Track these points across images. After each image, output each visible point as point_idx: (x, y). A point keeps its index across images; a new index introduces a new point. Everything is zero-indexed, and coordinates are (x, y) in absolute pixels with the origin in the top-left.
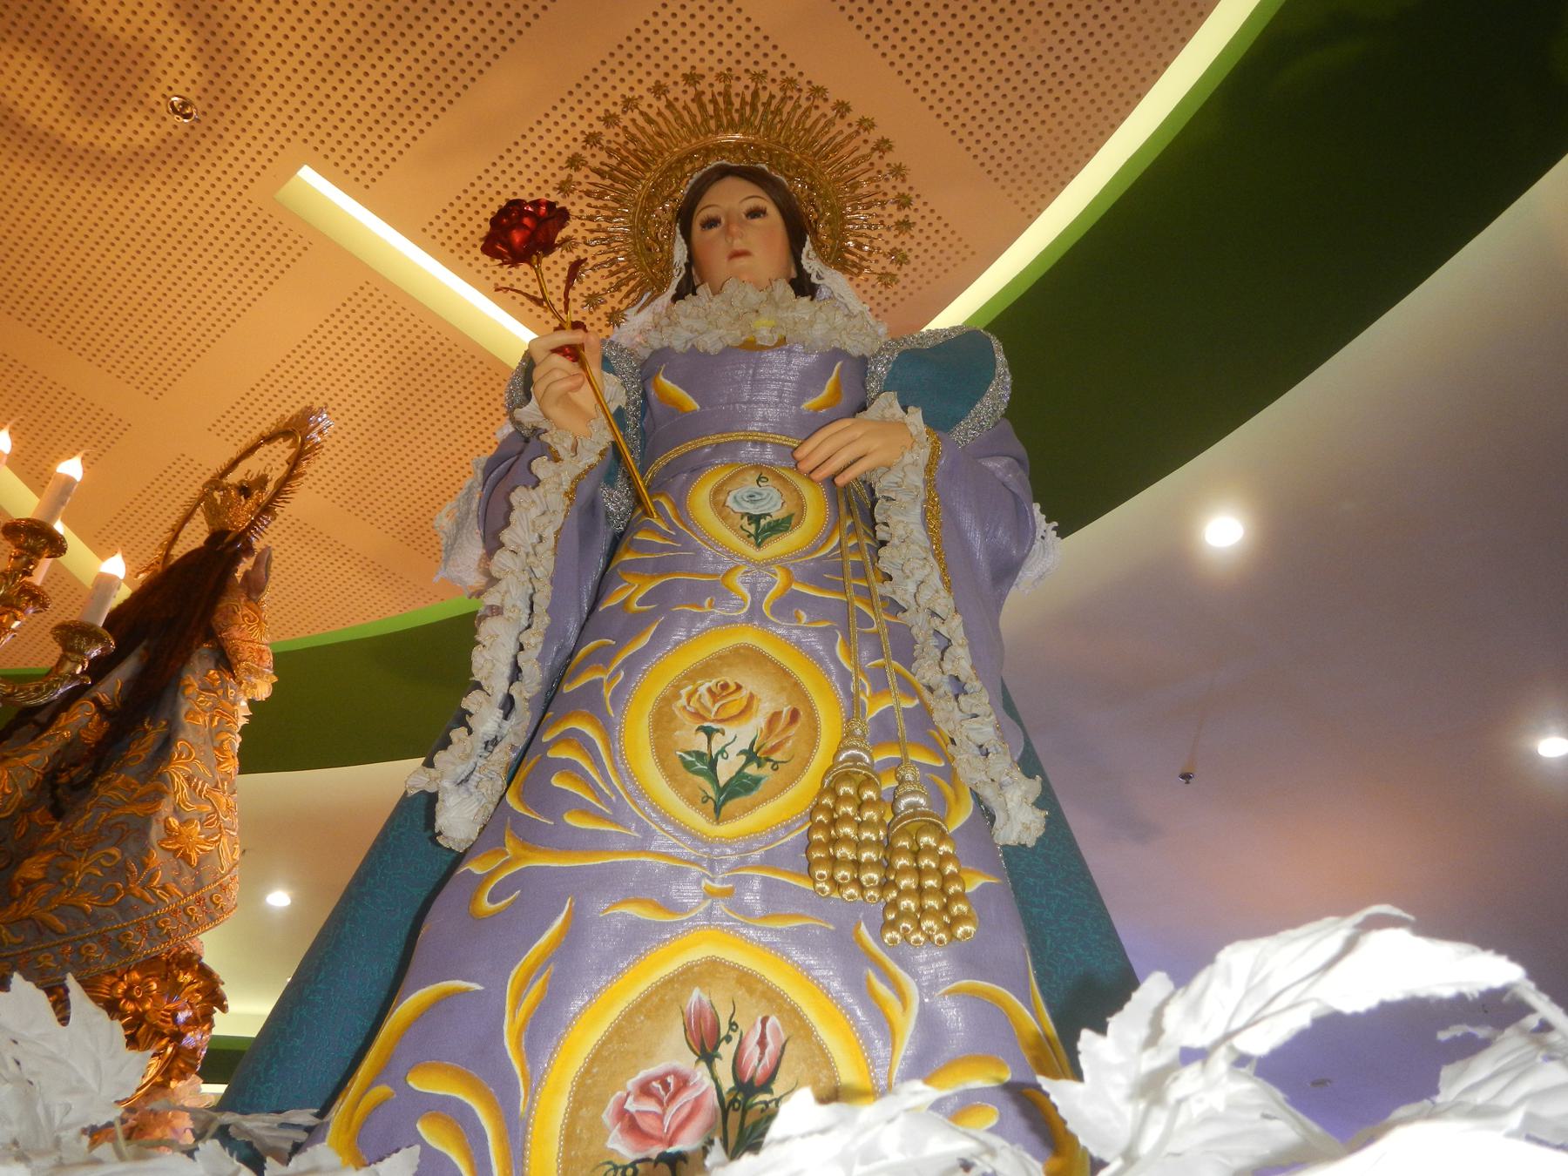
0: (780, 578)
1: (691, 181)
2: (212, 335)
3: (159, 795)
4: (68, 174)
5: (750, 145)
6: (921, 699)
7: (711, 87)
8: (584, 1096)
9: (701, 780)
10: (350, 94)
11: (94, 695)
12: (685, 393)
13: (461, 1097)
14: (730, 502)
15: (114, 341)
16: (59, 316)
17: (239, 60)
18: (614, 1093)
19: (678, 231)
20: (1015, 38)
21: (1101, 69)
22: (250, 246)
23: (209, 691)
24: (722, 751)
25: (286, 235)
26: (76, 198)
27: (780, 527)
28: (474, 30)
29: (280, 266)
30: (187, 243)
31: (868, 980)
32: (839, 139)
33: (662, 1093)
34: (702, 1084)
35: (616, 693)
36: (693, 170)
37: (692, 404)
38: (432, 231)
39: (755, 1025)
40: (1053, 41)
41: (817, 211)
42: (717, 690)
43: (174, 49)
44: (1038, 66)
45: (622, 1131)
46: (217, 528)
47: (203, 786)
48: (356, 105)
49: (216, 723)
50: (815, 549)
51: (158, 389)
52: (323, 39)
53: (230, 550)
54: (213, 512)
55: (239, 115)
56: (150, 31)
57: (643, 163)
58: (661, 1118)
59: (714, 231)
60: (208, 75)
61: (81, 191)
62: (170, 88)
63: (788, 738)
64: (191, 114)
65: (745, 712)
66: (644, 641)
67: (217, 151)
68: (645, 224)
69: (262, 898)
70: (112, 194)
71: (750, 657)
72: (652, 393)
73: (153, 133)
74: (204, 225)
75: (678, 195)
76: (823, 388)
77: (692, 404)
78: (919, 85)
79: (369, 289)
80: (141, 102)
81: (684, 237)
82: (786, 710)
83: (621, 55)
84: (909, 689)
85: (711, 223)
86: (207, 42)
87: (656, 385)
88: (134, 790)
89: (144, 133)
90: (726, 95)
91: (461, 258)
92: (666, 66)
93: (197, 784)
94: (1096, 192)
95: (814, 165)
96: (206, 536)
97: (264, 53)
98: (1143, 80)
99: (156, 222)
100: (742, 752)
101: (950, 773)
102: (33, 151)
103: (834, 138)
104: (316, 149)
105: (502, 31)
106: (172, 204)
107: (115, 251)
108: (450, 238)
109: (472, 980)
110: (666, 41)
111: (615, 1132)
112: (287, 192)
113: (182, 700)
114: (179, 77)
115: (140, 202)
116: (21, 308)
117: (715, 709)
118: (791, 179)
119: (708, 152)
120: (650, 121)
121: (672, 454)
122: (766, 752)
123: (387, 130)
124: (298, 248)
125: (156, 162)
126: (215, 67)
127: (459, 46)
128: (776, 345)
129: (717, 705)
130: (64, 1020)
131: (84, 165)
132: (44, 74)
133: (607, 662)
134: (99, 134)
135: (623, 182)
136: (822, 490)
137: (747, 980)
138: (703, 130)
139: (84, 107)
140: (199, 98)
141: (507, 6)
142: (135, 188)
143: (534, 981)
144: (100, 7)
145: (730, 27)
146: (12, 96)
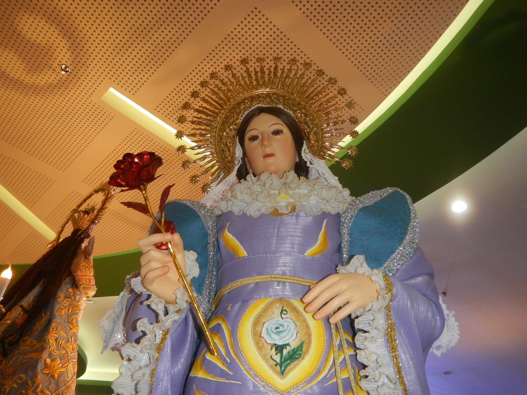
1: (244, 116)
2: (81, 149)
3: (42, 349)
4: (26, 94)
5: (274, 94)
7: (253, 65)
10: (143, 55)
11: (21, 304)
12: (239, 244)
14: (264, 334)
15: (46, 154)
17: (84, 50)
19: (238, 141)
20: (380, 28)
21: (421, 38)
22: (93, 117)
23: (68, 298)
25: (105, 113)
26: (30, 102)
29: (104, 124)
30: (70, 117)
32: (319, 89)
36: (245, 109)
37: (243, 252)
38: (158, 109)
40: (395, 28)
41: (309, 128)
43: (60, 47)
44: (389, 38)
46: (76, 228)
47: (62, 342)
48: (128, 65)
49: (70, 311)
50: (319, 372)
51: (63, 168)
53: (79, 238)
54: (75, 222)
55: (86, 70)
56: (51, 41)
59: (256, 142)
60: (74, 56)
61: (31, 100)
64: (68, 71)
67: (79, 83)
68: (221, 138)
70: (42, 100)
72: (221, 241)
74: (76, 110)
76: (317, 240)
77: (243, 252)
78: (322, 28)
79: (136, 131)
80: (50, 67)
83: (226, 42)
85: (254, 138)
86: (72, 44)
88: (34, 345)
89: (52, 78)
91: (169, 119)
92: (231, 57)
93: (59, 342)
95: (307, 103)
97: (93, 47)
99: (59, 110)
102: (13, 86)
104: (114, 81)
106: (64, 103)
107: (45, 120)
112: (107, 94)
113: (56, 304)
114: (63, 57)
115: (52, 103)
116: (14, 142)
118: (295, 111)
119: (252, 99)
120: (224, 84)
124: (110, 117)
125: (57, 89)
126: (76, 53)
127: (165, 41)
128: (290, 213)
131: (32, 91)
132: (15, 59)
134: (36, 79)
138: (250, 87)
139: (30, 70)
140: (71, 65)
142: (50, 98)
145: (267, 29)
146: (4, 67)
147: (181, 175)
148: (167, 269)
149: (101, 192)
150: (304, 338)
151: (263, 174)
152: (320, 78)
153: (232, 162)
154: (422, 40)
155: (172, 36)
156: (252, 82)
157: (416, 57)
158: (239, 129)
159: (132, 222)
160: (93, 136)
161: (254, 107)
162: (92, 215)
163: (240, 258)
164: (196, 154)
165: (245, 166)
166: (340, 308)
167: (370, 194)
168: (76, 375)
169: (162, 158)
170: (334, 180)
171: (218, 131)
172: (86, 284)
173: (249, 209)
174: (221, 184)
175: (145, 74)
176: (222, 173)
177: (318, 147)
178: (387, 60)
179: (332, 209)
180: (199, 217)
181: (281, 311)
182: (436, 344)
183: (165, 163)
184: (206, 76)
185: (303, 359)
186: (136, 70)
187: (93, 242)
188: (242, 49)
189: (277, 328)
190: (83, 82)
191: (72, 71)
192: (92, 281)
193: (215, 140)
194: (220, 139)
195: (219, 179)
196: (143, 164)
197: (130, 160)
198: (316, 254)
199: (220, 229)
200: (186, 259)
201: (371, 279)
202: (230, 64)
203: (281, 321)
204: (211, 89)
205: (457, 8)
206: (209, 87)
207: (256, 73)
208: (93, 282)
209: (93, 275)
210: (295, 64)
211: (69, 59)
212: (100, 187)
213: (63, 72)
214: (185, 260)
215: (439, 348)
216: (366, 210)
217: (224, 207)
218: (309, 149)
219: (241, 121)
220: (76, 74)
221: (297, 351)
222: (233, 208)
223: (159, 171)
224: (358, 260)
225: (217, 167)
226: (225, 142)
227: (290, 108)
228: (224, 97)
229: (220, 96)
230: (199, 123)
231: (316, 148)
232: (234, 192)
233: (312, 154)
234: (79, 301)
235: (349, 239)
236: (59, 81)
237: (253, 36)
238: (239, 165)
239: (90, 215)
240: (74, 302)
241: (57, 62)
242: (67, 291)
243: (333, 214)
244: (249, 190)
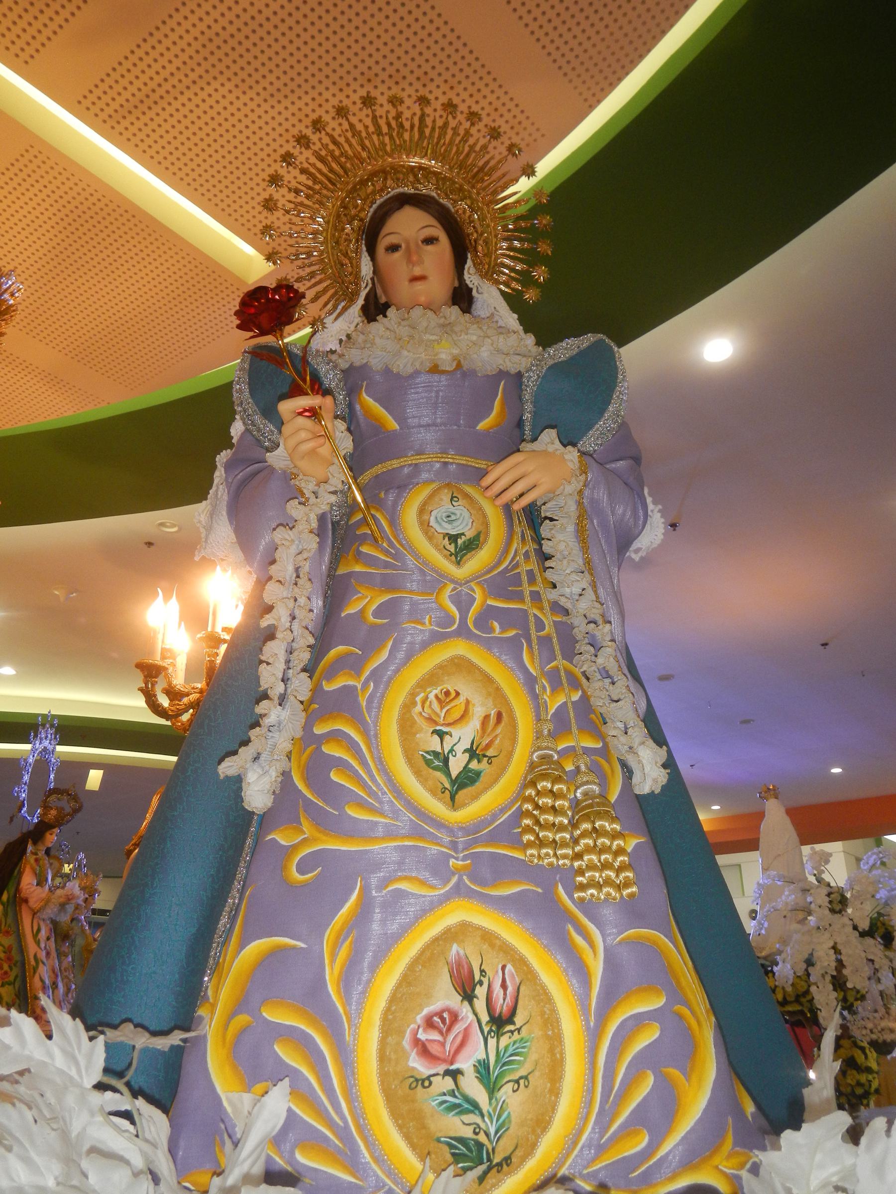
0: (478, 595)
1: (375, 206)
6: (584, 691)
8: (389, 1027)
9: (438, 774)
13: (303, 1027)
14: (433, 523)
18: (408, 1026)
19: (364, 248)
24: (452, 750)
27: (473, 545)
31: (568, 932)
32: (492, 163)
33: (442, 1026)
34: (468, 1017)
35: (370, 701)
39: (497, 972)
41: (477, 232)
42: (441, 696)
45: (417, 1053)
50: (499, 563)
58: (443, 1044)
59: (397, 255)
63: (496, 736)
65: (464, 716)
66: (384, 655)
68: (337, 243)
71: (460, 665)
72: (358, 407)
76: (492, 409)
77: (392, 424)
82: (493, 713)
84: (575, 684)
85: (393, 248)
91: (129, 140)
100: (465, 751)
101: (604, 751)
109: (298, 940)
111: (413, 1054)
117: (443, 715)
119: (384, 172)
120: (335, 142)
121: (378, 469)
122: (482, 750)
129: (444, 710)
130: (50, 1037)
133: (357, 670)
136: (500, 511)
137: (488, 936)
138: (381, 153)
143: (342, 943)
150: (481, 528)
152: (494, 143)
159: (25, 364)
166: (521, 495)
167: (564, 344)
170: (511, 320)
174: (340, 319)
175: (180, 107)
177: (489, 265)
182: (636, 545)
185: (481, 548)
189: (449, 516)
195: (338, 311)
198: (491, 428)
202: (344, 104)
203: (452, 509)
215: (637, 551)
216: (558, 369)
217: (355, 356)
221: (474, 540)
224: (549, 437)
231: (486, 266)
235: (533, 409)
238: (368, 289)
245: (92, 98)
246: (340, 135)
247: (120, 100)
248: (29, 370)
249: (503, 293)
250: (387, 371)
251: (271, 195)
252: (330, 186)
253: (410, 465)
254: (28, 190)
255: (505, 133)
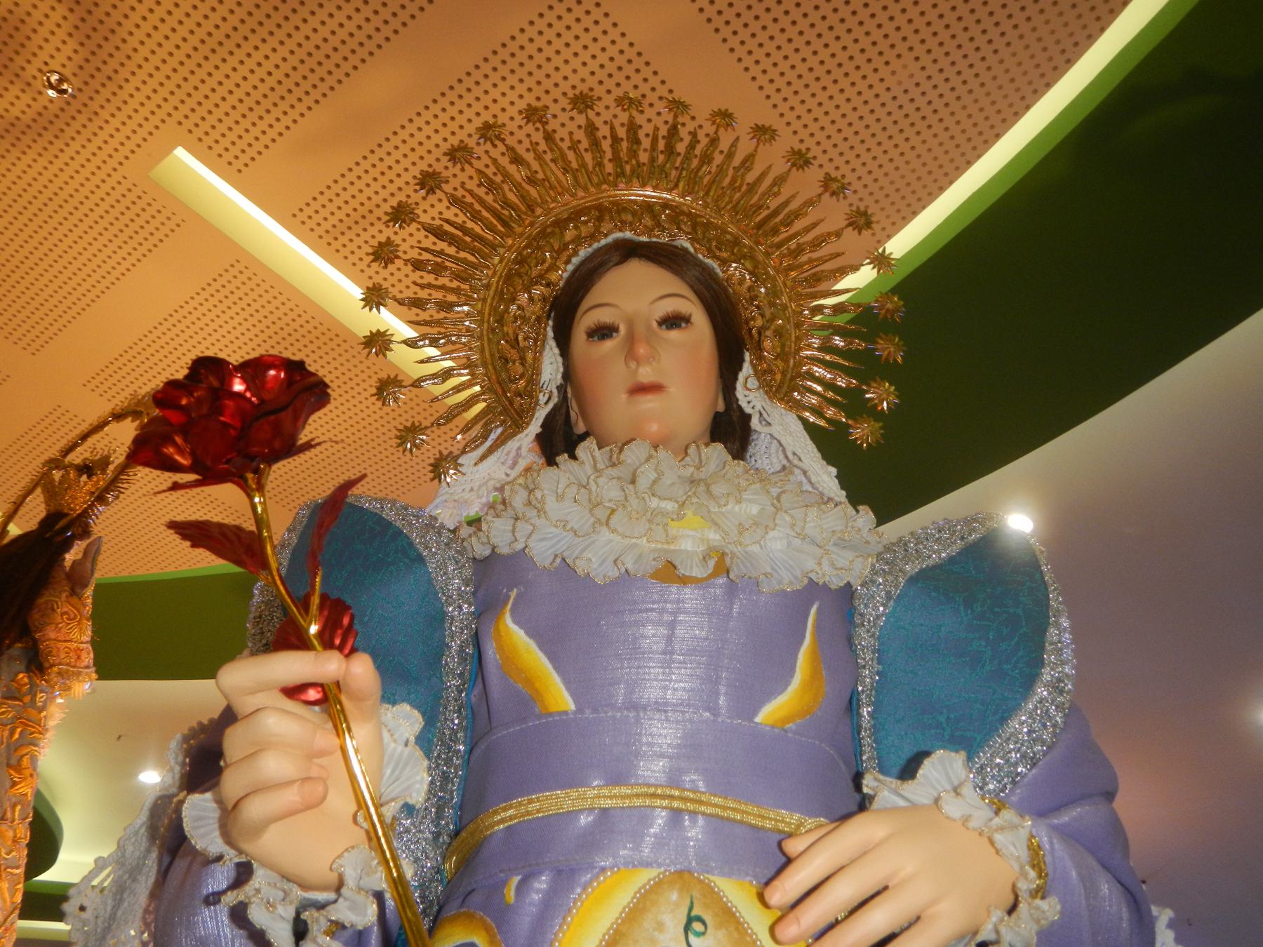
1: (575, 260)
7: (608, 115)
16: (43, 233)
17: (115, 40)
19: (550, 334)
28: (350, 26)
32: (793, 206)
36: (578, 241)
41: (763, 316)
43: (49, 25)
46: (52, 509)
49: (16, 736)
51: (35, 346)
52: (199, 25)
53: (59, 539)
54: (52, 493)
57: (504, 223)
59: (609, 345)
60: (84, 53)
62: (46, 64)
64: (65, 91)
67: (92, 127)
68: (500, 321)
69: (136, 775)
73: (29, 106)
75: (553, 277)
77: (560, 698)
79: (239, 267)
80: (17, 75)
81: (559, 345)
83: (495, 61)
85: (603, 332)
87: (498, 638)
89: (21, 105)
90: (633, 128)
94: (940, 221)
96: (43, 514)
97: (139, 35)
98: (1004, 120)
103: (786, 203)
105: (378, 30)
108: (375, 179)
110: (540, 50)
118: (724, 263)
119: (601, 212)
120: (517, 160)
123: (292, 107)
124: (171, 224)
126: (91, 45)
135: (472, 251)
138: (595, 180)
140: (75, 75)
141: (385, 4)
144: (154, 7)
145: (604, 41)
147: (313, 352)
148: (320, 789)
149: (130, 419)
151: (632, 445)
153: (530, 392)
154: (984, 114)
155: (347, 38)
156: (600, 165)
157: (963, 154)
158: (555, 298)
160: (101, 287)
161: (610, 239)
162: (101, 480)
163: (550, 714)
164: (422, 362)
165: (564, 411)
168: (17, 912)
169: (327, 380)
170: (826, 478)
171: (493, 298)
172: (68, 664)
173: (585, 555)
174: (492, 459)
176: (497, 427)
177: (784, 373)
178: (894, 153)
179: (835, 572)
180: (420, 559)
181: (684, 921)
183: (335, 399)
184: (467, 134)
186: (251, 109)
187: (98, 552)
188: (534, 86)
190: (104, 125)
191: (76, 93)
192: (84, 655)
193: (480, 323)
194: (497, 321)
195: (488, 443)
196: (262, 401)
197: (215, 383)
198: (789, 719)
199: (487, 608)
200: (386, 735)
201: (992, 842)
204: (479, 172)
205: (1076, 44)
206: (471, 164)
207: (616, 140)
208: (88, 658)
209: (88, 639)
210: (728, 125)
211: (70, 59)
212: (129, 404)
213: (51, 93)
214: (381, 738)
217: (500, 534)
218: (758, 379)
219: (566, 275)
220: (89, 102)
222: (531, 544)
223: (316, 426)
225: (480, 406)
226: (511, 332)
227: (709, 250)
228: (516, 201)
229: (504, 196)
230: (438, 270)
231: (778, 377)
232: (538, 494)
233: (766, 392)
234: (43, 709)
236: (40, 114)
237: (566, 53)
238: (550, 406)
239: (95, 478)
240: (30, 709)
241: (36, 62)
242: (13, 681)
243: (833, 587)
244: (583, 490)
245: (309, 211)
246: (528, 150)
247: (340, 215)
248: (214, 505)
249: (810, 428)
250: (565, 569)
251: (389, 238)
252: (500, 228)
253: (591, 810)
254: (229, 308)
255: (815, 158)
